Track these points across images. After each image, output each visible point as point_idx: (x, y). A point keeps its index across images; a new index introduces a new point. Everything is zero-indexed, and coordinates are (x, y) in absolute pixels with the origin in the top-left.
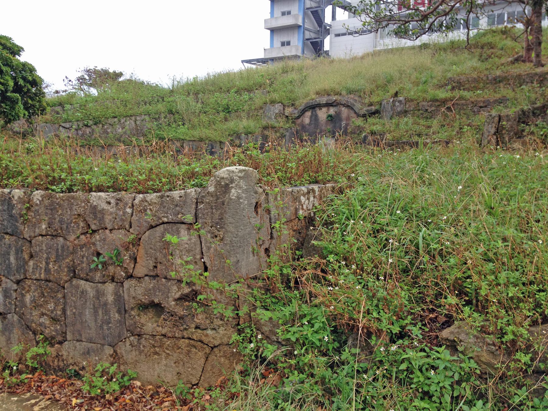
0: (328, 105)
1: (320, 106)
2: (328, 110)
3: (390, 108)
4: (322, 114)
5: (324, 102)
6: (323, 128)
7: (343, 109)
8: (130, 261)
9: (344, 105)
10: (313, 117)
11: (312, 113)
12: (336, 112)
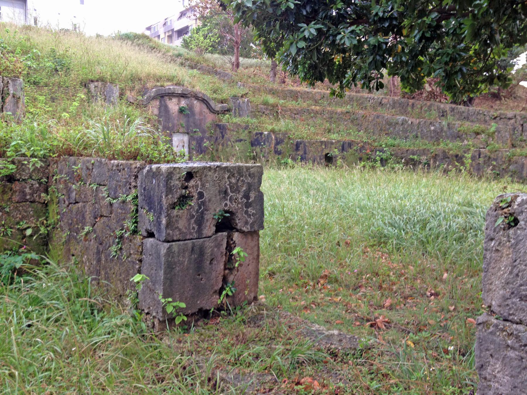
0: (183, 96)
1: (171, 95)
2: (179, 101)
4: (173, 105)
5: (180, 92)
6: (176, 122)
7: (195, 102)
8: (388, 163)
9: (197, 98)
11: (160, 102)
12: (187, 105)
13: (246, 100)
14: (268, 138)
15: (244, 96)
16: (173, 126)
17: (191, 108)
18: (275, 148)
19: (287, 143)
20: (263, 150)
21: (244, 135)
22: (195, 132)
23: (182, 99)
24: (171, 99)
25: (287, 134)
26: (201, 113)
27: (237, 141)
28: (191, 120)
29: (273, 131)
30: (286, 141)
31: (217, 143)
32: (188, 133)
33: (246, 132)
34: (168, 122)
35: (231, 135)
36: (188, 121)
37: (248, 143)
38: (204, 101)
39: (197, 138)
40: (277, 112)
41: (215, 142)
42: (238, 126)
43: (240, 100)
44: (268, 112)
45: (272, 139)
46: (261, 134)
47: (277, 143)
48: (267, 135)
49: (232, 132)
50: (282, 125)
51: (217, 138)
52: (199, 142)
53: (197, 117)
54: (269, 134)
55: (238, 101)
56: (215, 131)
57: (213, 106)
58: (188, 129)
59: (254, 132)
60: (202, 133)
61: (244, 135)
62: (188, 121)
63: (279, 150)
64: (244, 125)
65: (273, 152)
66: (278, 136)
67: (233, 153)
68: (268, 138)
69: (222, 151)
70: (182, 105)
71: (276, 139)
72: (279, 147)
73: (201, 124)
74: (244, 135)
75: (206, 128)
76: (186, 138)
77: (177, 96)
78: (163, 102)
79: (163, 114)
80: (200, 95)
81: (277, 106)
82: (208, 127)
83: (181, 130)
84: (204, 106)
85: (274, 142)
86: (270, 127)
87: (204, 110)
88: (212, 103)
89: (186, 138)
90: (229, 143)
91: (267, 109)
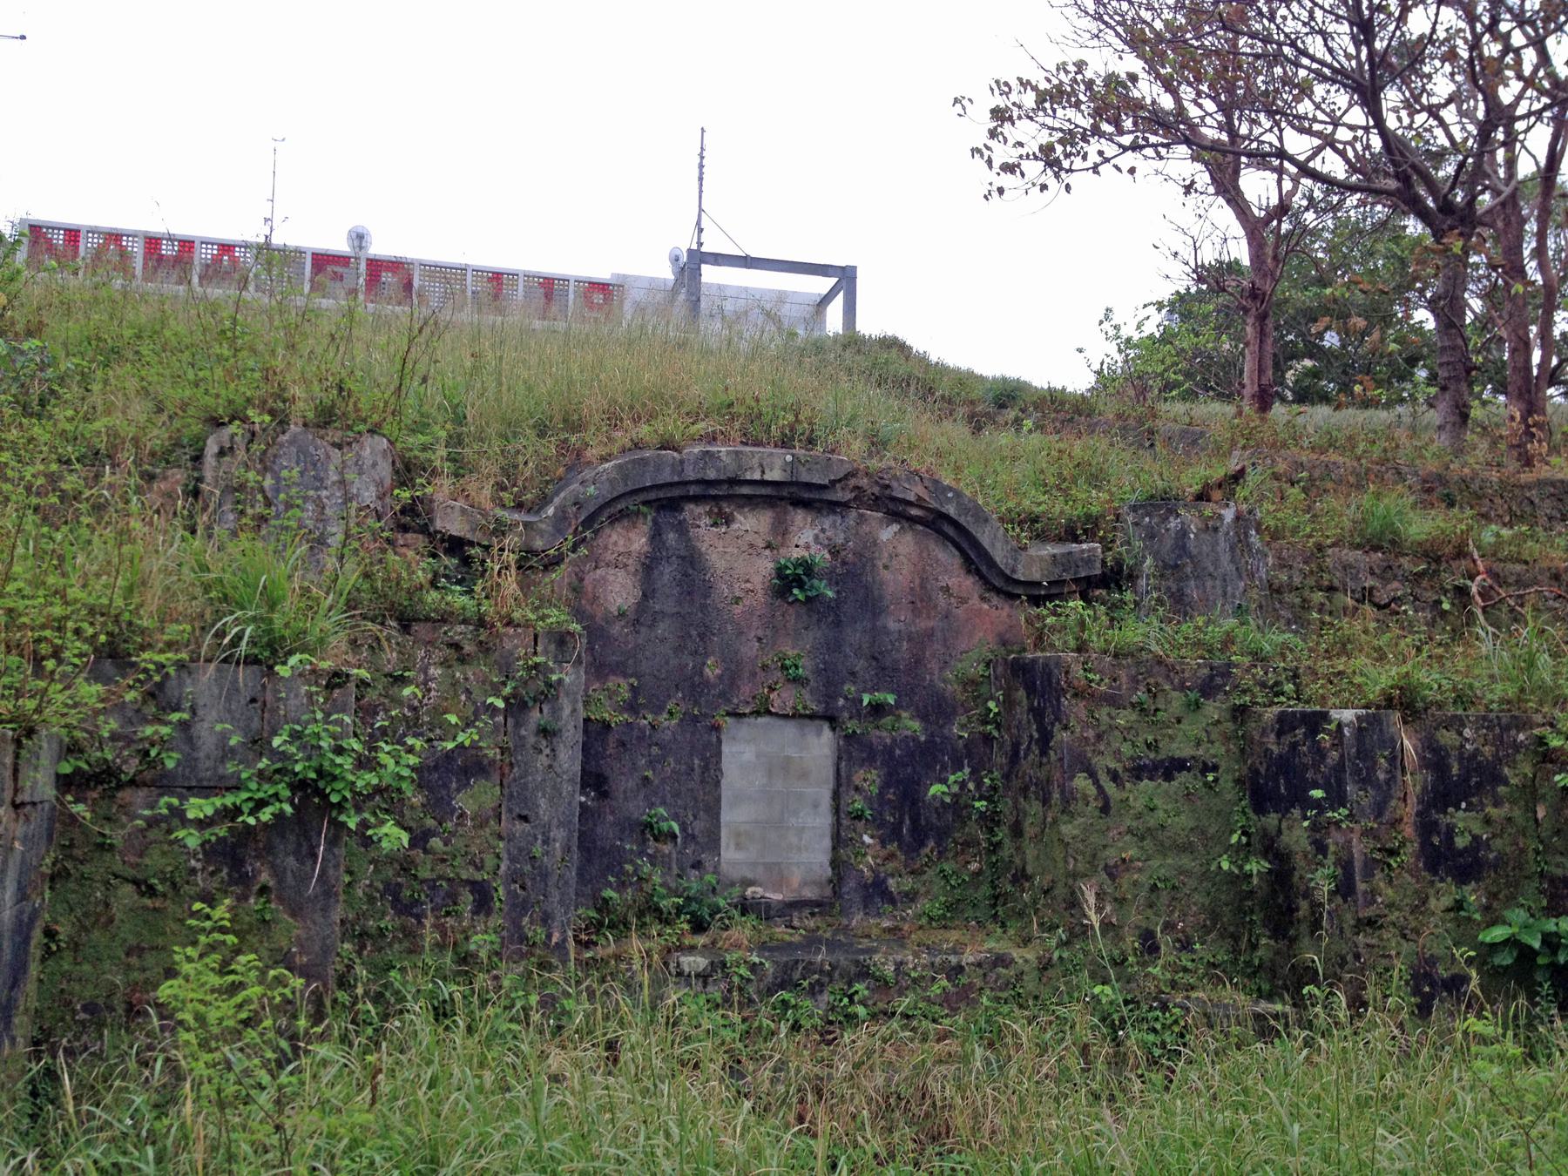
1: (725, 494)
2: (781, 530)
3: (1225, 559)
4: (739, 554)
5: (775, 475)
6: (749, 649)
7: (888, 533)
9: (895, 509)
10: (667, 573)
11: (656, 536)
12: (834, 552)
13: (1229, 515)
14: (1364, 753)
15: (1217, 495)
16: (732, 679)
17: (853, 572)
18: (1426, 827)
19: (1530, 793)
20: (1333, 841)
21: (1194, 732)
22: (878, 709)
23: (799, 517)
24: (729, 521)
25: (1523, 724)
26: (921, 599)
27: (1139, 772)
28: (855, 636)
29: (1405, 701)
30: (1519, 771)
31: (1016, 783)
32: (832, 720)
33: (1214, 709)
34: (700, 655)
35: (1103, 734)
36: (834, 646)
37: (1226, 782)
38: (941, 524)
39: (889, 751)
40: (1462, 592)
41: (1007, 777)
42: (1150, 670)
43: (1189, 519)
44: (1397, 588)
45: (1396, 760)
46: (1315, 721)
47: (1443, 794)
48: (1360, 732)
49: (1103, 713)
50: (1486, 664)
51: (1016, 746)
52: (905, 772)
53: (895, 622)
54: (1369, 727)
55: (1173, 523)
56: (1009, 703)
57: (999, 555)
58: (830, 690)
59: (1270, 714)
60: (923, 717)
61: (1193, 727)
62: (834, 646)
63: (1461, 842)
64: (1194, 661)
65: (1408, 855)
66: (1447, 738)
67: (1111, 855)
68: (1364, 753)
69: (1038, 838)
70: (796, 554)
71: (1435, 758)
72: (1464, 823)
73: (918, 661)
74: (1194, 732)
75: (953, 689)
76: (820, 746)
77: (768, 502)
78: (671, 537)
79: (670, 606)
80: (914, 491)
81: (1461, 553)
82: (969, 683)
83: (784, 699)
84: (947, 558)
85: (1414, 782)
86: (1382, 679)
87: (945, 580)
88: (989, 537)
89: (820, 746)
90: (1081, 782)
91: (1386, 572)
